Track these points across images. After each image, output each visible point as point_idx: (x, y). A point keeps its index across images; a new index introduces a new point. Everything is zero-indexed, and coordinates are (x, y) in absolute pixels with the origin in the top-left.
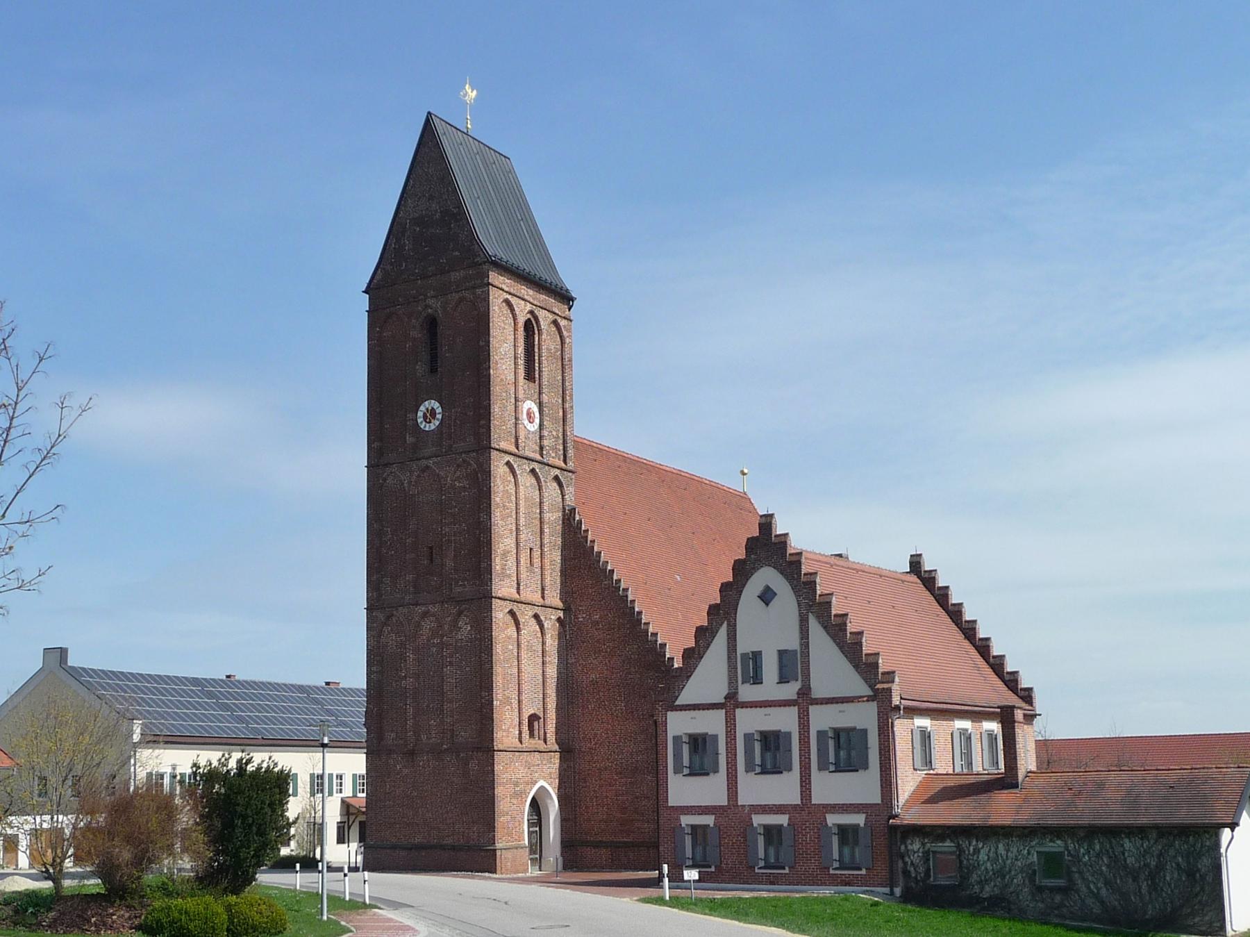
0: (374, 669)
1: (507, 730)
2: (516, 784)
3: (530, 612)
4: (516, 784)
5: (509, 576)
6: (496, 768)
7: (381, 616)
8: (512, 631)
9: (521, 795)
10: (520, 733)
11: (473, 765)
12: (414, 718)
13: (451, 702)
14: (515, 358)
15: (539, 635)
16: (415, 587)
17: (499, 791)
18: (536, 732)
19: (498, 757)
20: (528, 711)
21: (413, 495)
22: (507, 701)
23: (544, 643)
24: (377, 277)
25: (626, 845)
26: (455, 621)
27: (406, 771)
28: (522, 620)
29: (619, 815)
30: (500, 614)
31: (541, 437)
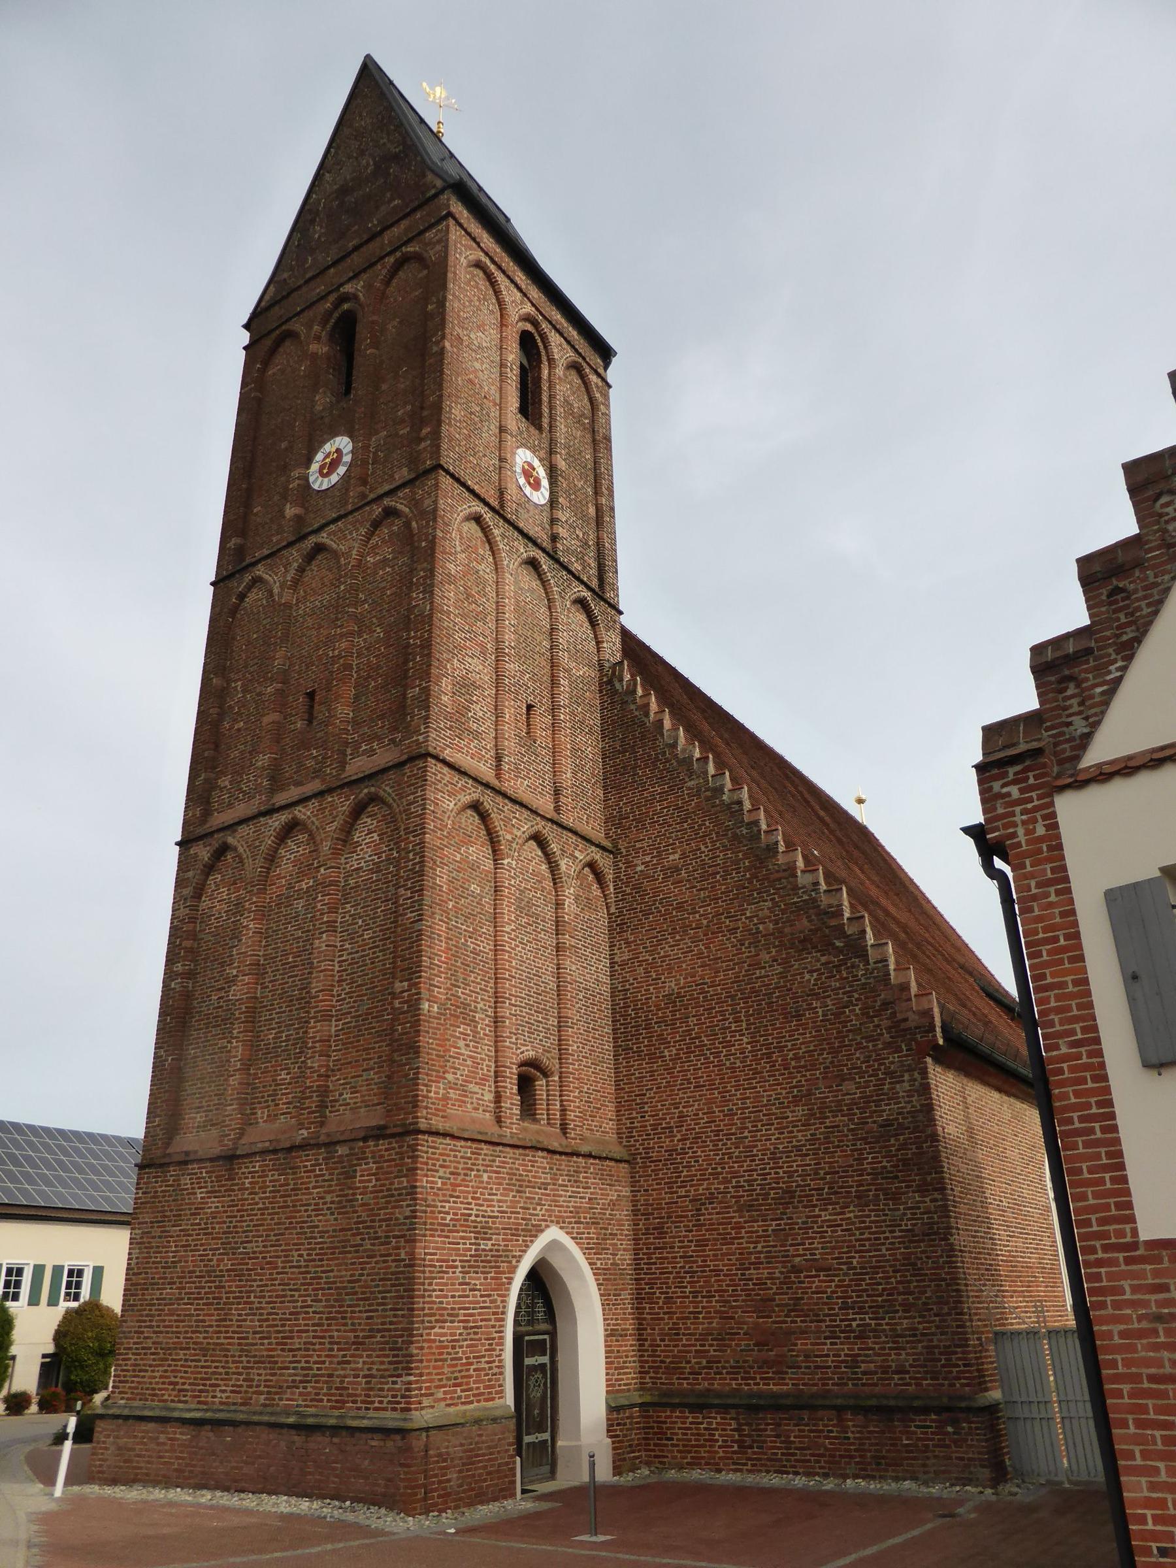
0: (179, 967)
1: (461, 1083)
2: (482, 1233)
3: (525, 826)
4: (482, 1233)
5: (476, 735)
6: (423, 1182)
7: (203, 852)
8: (478, 852)
9: (496, 1264)
10: (498, 1098)
11: (365, 1176)
12: (246, 1067)
13: (327, 1017)
14: (502, 365)
15: (548, 884)
16: (272, 779)
17: (431, 1248)
18: (541, 1108)
19: (427, 1147)
20: (520, 1049)
21: (288, 606)
22: (462, 1013)
23: (559, 905)
24: (267, 297)
25: (776, 1405)
26: (348, 829)
27: (214, 1204)
28: (505, 836)
29: (751, 1319)
30: (446, 800)
31: (553, 521)
